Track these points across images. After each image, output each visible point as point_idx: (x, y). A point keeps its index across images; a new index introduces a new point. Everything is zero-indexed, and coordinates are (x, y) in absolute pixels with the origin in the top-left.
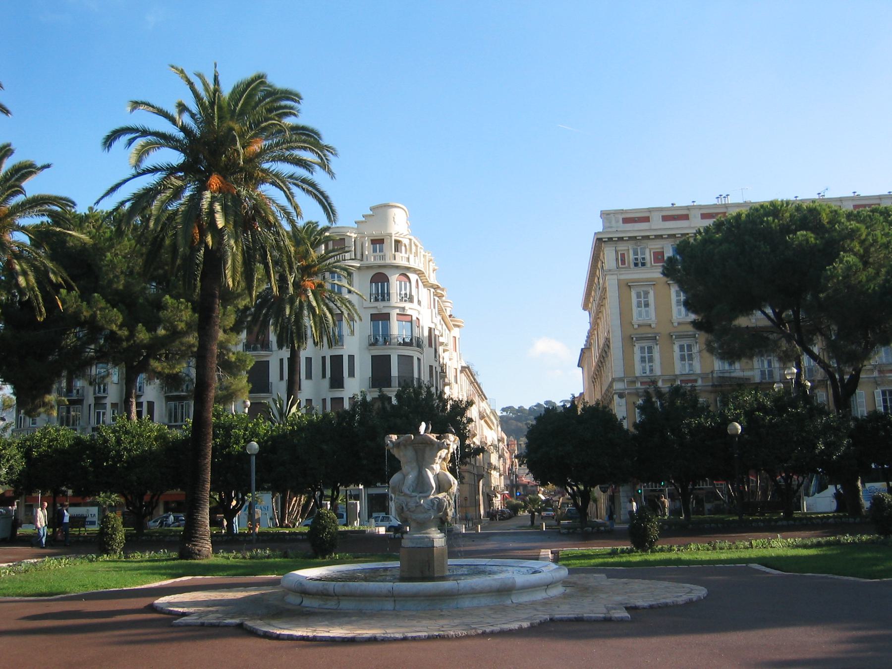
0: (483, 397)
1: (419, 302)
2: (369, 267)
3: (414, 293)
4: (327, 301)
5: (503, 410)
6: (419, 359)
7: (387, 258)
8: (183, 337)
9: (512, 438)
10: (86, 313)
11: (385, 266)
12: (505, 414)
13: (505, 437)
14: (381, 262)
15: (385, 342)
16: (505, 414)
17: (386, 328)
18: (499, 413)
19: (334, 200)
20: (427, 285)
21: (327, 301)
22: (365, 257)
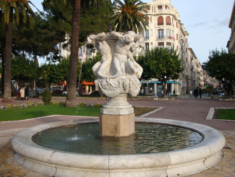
0: (196, 58)
1: (173, 26)
2: (157, 15)
3: (171, 22)
4: (146, 146)
5: (203, 63)
6: (173, 43)
7: (163, 11)
8: (123, 5)
9: (205, 71)
10: (29, 42)
11: (162, 14)
12: (203, 64)
13: (203, 70)
14: (161, 13)
15: (162, 37)
16: (203, 64)
17: (163, 33)
18: (202, 65)
19: (31, 1)
20: (176, 19)
21: (146, 146)
22: (156, 11)
